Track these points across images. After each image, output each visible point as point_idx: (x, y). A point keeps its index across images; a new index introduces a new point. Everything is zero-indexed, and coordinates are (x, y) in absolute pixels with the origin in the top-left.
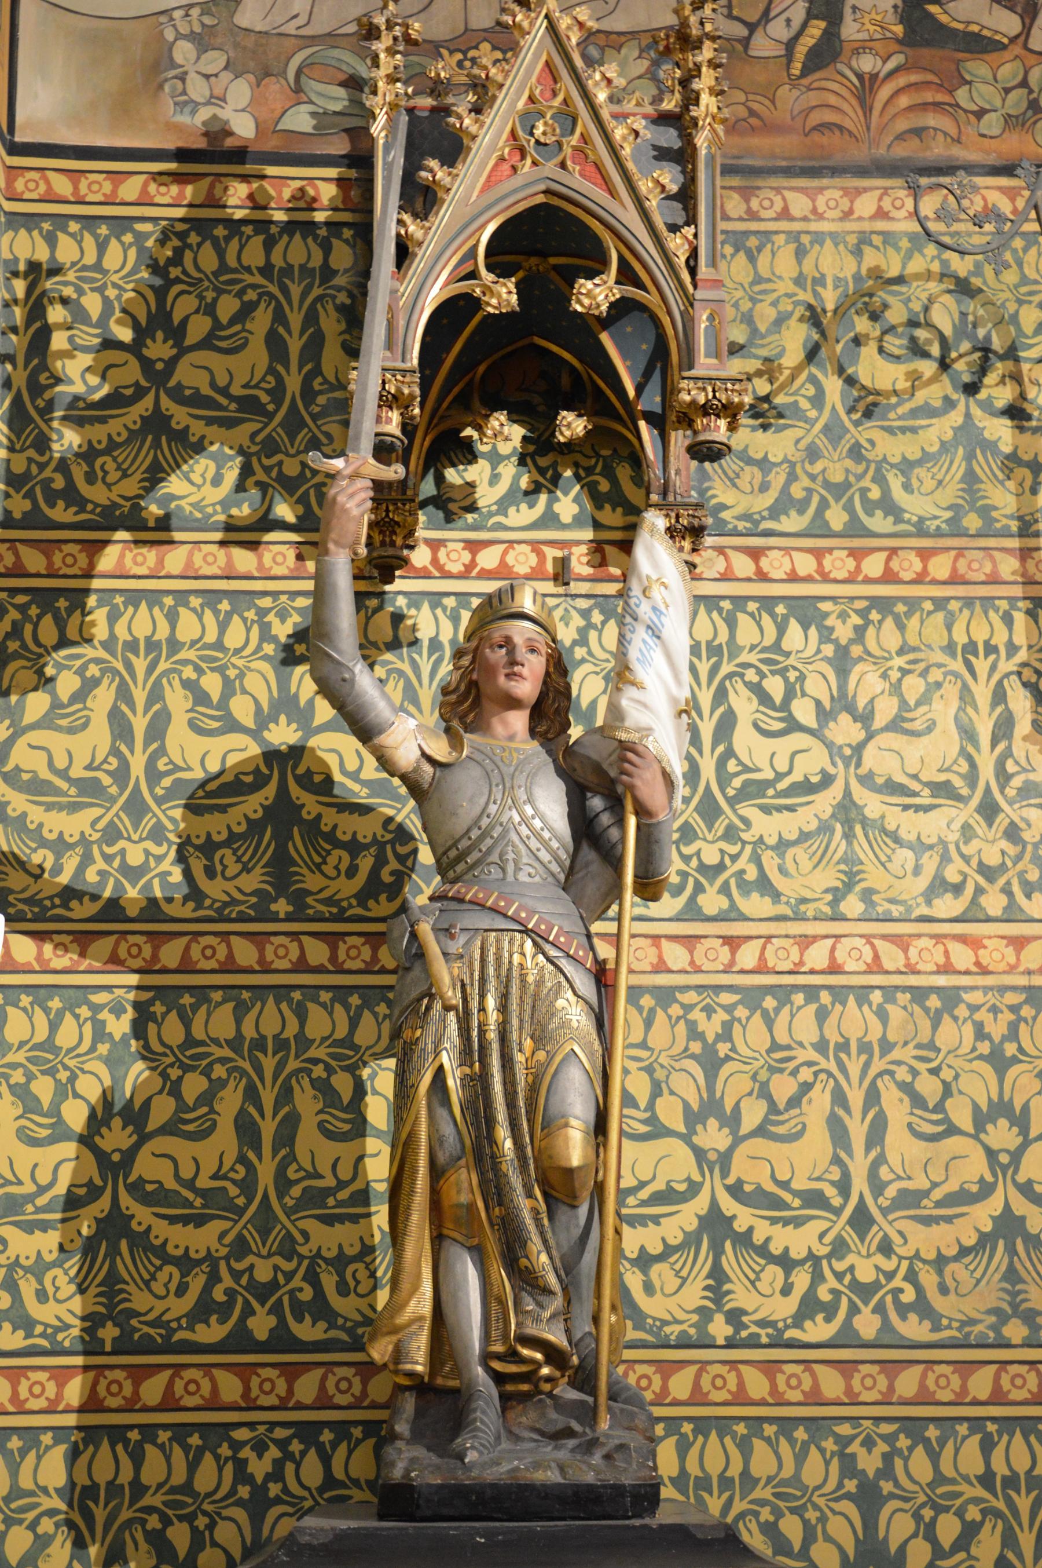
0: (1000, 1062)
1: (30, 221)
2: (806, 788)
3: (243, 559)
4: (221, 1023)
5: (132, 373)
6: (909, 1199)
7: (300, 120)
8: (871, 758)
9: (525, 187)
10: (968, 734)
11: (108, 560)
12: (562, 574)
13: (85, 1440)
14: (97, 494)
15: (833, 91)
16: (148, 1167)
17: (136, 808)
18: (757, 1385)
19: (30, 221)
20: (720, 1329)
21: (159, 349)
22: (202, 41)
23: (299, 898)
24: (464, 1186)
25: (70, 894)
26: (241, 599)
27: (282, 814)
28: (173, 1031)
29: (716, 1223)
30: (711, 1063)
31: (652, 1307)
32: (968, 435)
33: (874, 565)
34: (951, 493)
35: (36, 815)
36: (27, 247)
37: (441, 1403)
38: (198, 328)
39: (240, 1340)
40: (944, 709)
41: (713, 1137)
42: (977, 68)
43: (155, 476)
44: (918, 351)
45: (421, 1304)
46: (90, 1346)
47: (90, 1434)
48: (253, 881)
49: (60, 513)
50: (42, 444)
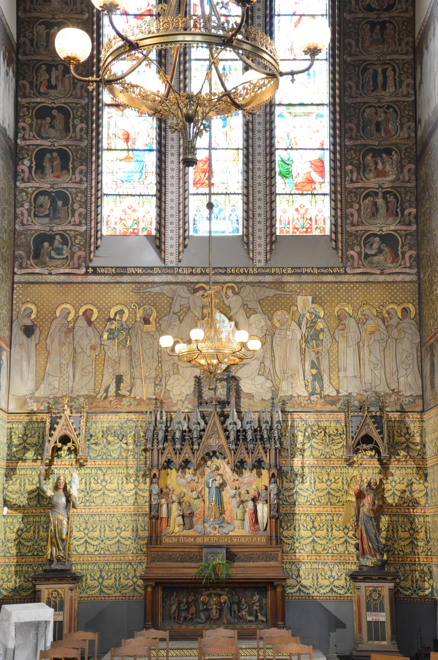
0: (119, 522)
1: (10, 422)
2: (99, 490)
3: (35, 464)
4: (31, 519)
5: (22, 441)
6: (108, 538)
7: (42, 408)
8: (107, 487)
9: (62, 433)
10: (118, 484)
11: (19, 464)
12: (72, 465)
13: (16, 566)
14: (17, 456)
15: (107, 402)
16: (23, 536)
17: (22, 494)
18: (90, 559)
19: (10, 422)
20: (86, 553)
21: (25, 438)
22: (31, 398)
23: (40, 505)
24: (54, 540)
25: (15, 505)
26: (34, 469)
27: (39, 495)
28: (26, 520)
29: (86, 541)
30: (87, 523)
31: (78, 551)
32: (121, 447)
33: (108, 463)
34: (118, 454)
35: (11, 495)
36: (10, 425)
37: (51, 561)
38: (30, 435)
39: (33, 555)
40: (116, 481)
41: (86, 531)
42: (124, 399)
43: (24, 454)
44: (115, 436)
45: (50, 552)
46: (17, 556)
47: (17, 565)
48: (35, 503)
49: (13, 459)
50: (11, 450)
